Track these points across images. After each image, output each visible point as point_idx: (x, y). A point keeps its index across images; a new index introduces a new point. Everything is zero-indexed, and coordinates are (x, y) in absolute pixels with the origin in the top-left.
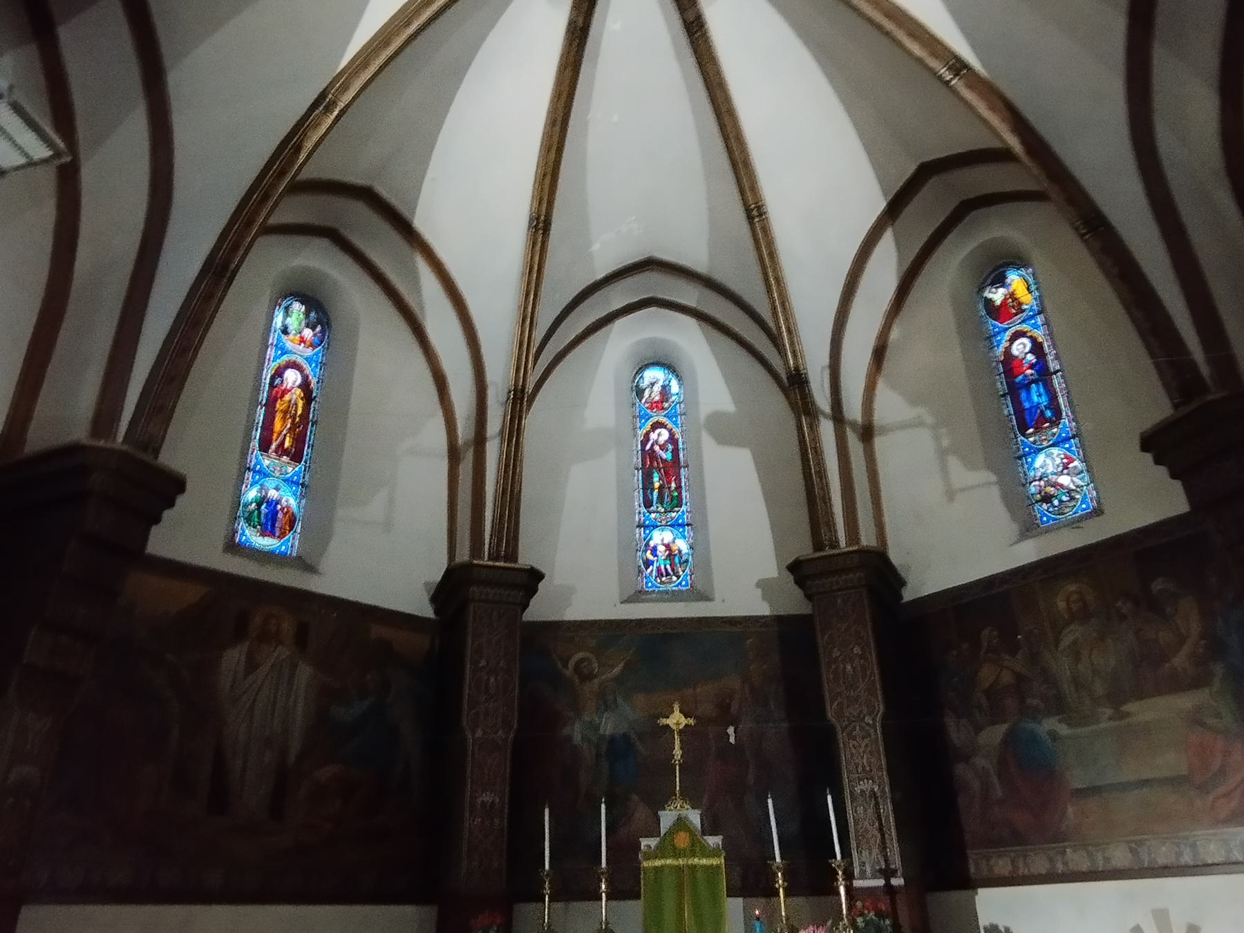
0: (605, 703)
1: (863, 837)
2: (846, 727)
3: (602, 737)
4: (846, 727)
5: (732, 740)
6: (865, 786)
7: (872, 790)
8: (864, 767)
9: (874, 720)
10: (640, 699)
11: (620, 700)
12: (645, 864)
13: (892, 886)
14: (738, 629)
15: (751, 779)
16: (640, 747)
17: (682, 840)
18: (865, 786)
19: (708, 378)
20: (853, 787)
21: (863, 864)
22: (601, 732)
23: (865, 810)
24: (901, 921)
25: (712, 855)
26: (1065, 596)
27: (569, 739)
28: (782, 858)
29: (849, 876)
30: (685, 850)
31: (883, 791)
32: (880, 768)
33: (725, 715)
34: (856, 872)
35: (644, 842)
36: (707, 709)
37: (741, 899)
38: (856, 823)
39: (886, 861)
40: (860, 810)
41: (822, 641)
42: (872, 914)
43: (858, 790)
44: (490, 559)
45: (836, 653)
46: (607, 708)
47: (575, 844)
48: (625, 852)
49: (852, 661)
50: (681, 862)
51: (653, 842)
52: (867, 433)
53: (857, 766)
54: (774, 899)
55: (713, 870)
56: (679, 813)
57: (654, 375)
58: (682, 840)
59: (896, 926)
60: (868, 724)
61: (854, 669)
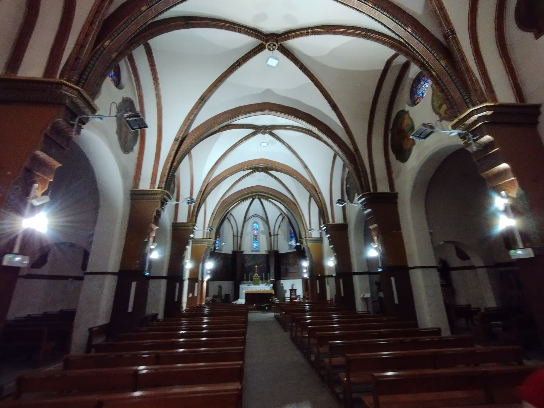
19: (261, 226)
25: (259, 278)
26: (291, 255)
44: (62, 76)
47: (247, 277)
48: (252, 276)
52: (277, 235)
56: (256, 275)
57: (255, 224)
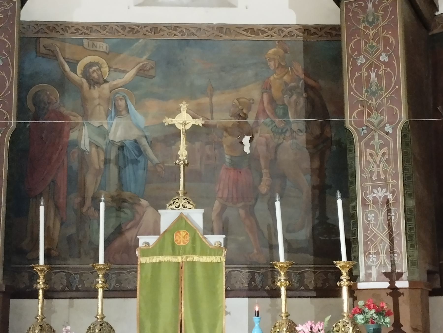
0: (116, 110)
1: (372, 242)
2: (366, 135)
3: (112, 143)
4: (366, 135)
5: (247, 149)
6: (380, 193)
7: (386, 196)
8: (378, 174)
9: (395, 129)
10: (153, 106)
11: (131, 107)
12: (142, 260)
13: (397, 289)
14: (261, 37)
15: (263, 189)
16: (150, 152)
17: (182, 238)
18: (380, 193)
20: (366, 194)
21: (368, 268)
22: (111, 137)
23: (376, 217)
24: (402, 322)
27: (76, 144)
28: (287, 258)
29: (353, 277)
30: (184, 247)
31: (396, 199)
32: (395, 177)
33: (241, 127)
34: (362, 274)
35: (143, 240)
36: (223, 118)
37: (247, 299)
38: (366, 229)
39: (393, 264)
40: (371, 217)
41: (346, 49)
42: (373, 311)
43: (370, 197)
45: (361, 60)
46: (118, 113)
47: (72, 245)
48: (123, 253)
49: (377, 67)
50: (180, 259)
51: (152, 240)
53: (372, 173)
54: (278, 299)
55: (210, 268)
56: (180, 214)
58: (182, 238)
59: (397, 324)
60: (387, 133)
61: (377, 75)
